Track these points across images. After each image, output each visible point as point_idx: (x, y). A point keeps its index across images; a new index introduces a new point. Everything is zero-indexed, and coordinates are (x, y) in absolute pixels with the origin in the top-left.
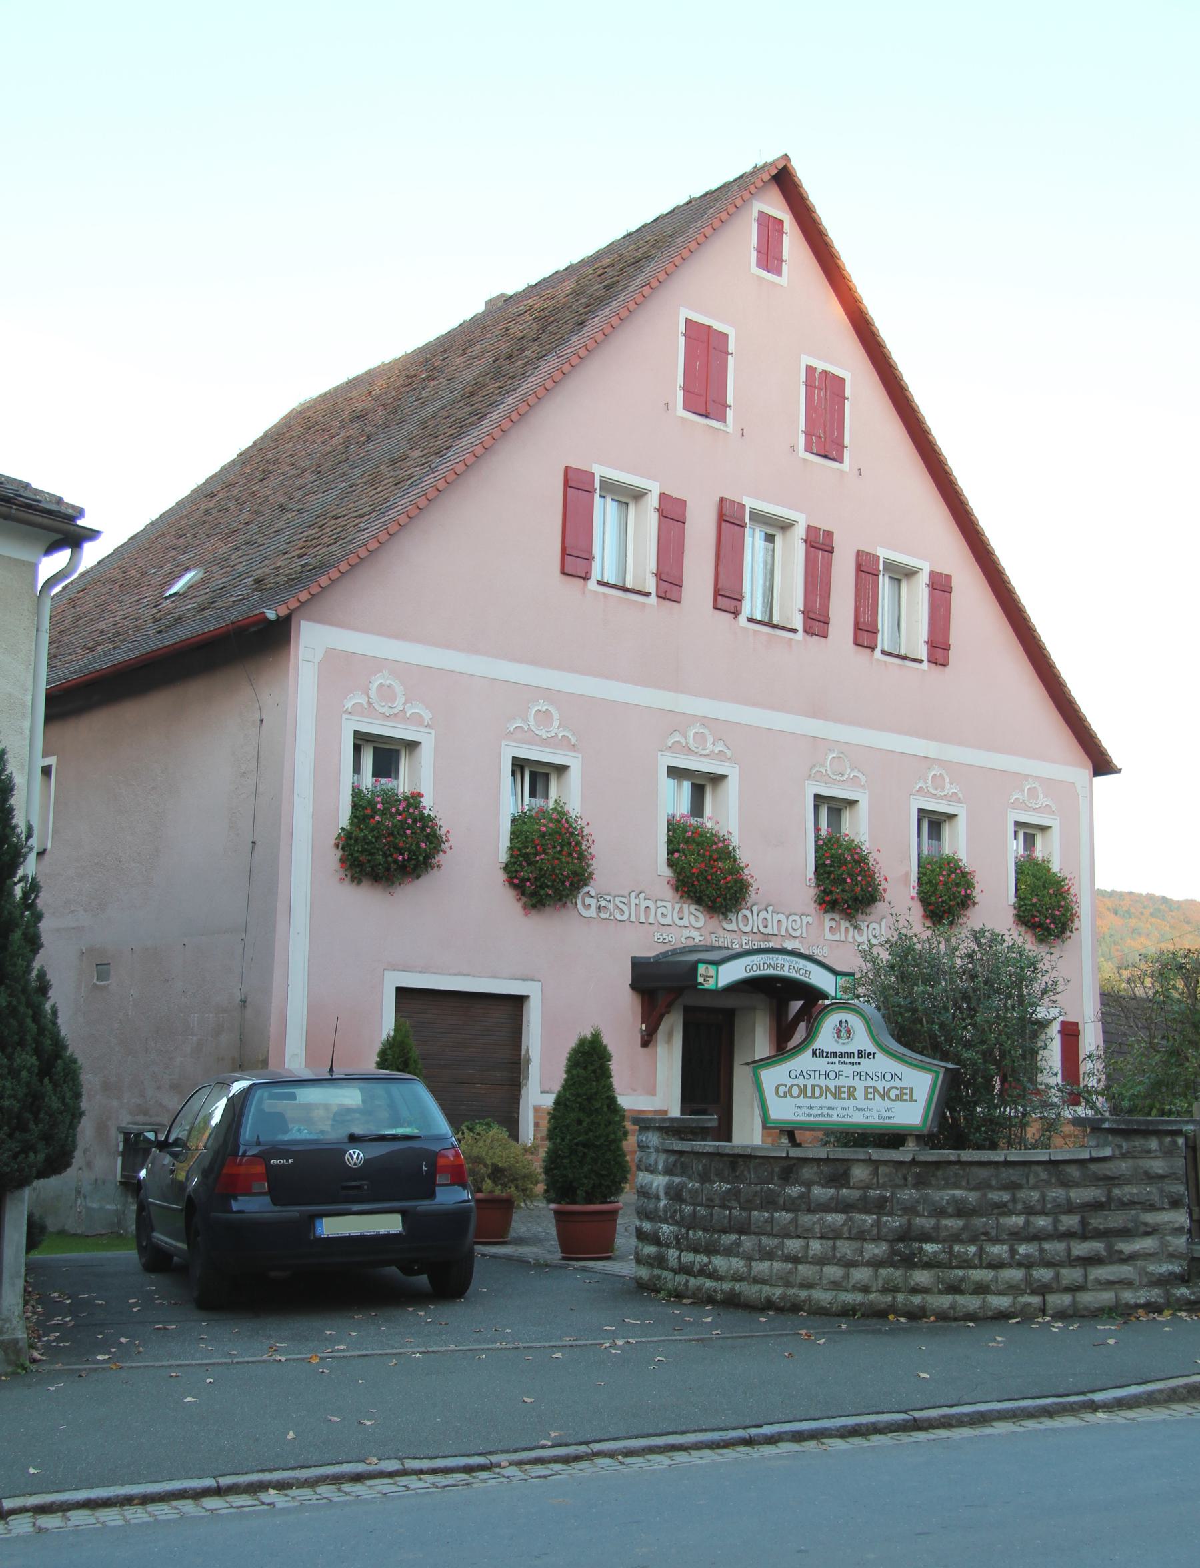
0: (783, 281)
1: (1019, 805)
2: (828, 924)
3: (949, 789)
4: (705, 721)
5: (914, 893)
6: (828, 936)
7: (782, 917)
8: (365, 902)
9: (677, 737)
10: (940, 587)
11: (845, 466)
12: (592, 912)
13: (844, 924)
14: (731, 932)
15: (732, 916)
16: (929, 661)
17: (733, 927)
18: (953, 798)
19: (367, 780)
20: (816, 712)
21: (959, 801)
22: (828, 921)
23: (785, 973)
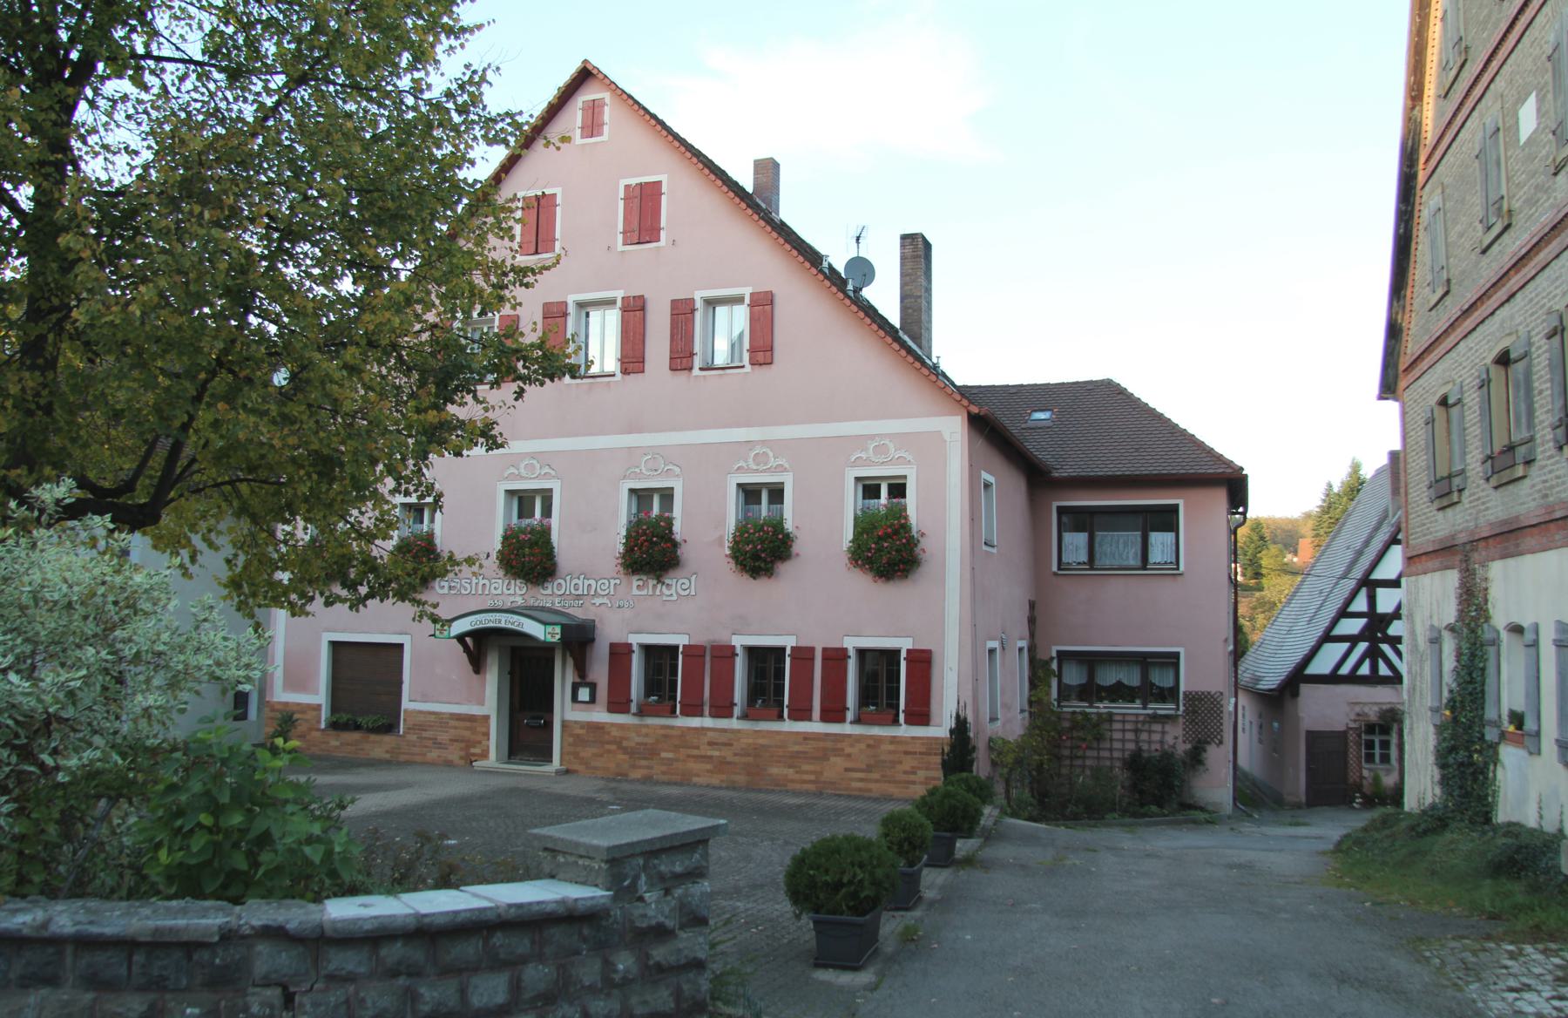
0: (605, 137)
1: (857, 463)
2: (635, 584)
3: (772, 463)
4: (533, 455)
5: (728, 552)
6: (635, 592)
7: (592, 582)
8: (861, 583)
9: (512, 470)
10: (762, 306)
11: (663, 242)
12: (446, 591)
13: (652, 582)
14: (548, 595)
15: (549, 585)
16: (752, 364)
17: (549, 591)
18: (781, 469)
19: (515, 519)
20: (631, 429)
21: (785, 470)
22: (635, 581)
23: (503, 625)
